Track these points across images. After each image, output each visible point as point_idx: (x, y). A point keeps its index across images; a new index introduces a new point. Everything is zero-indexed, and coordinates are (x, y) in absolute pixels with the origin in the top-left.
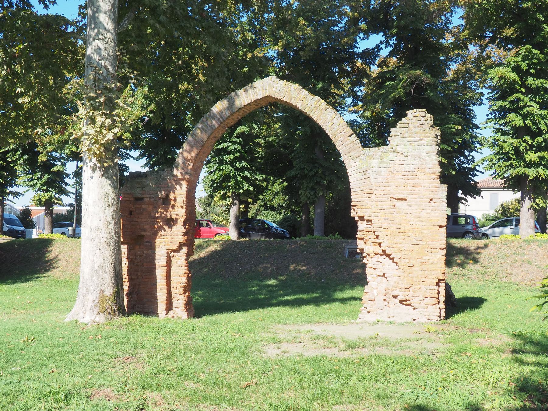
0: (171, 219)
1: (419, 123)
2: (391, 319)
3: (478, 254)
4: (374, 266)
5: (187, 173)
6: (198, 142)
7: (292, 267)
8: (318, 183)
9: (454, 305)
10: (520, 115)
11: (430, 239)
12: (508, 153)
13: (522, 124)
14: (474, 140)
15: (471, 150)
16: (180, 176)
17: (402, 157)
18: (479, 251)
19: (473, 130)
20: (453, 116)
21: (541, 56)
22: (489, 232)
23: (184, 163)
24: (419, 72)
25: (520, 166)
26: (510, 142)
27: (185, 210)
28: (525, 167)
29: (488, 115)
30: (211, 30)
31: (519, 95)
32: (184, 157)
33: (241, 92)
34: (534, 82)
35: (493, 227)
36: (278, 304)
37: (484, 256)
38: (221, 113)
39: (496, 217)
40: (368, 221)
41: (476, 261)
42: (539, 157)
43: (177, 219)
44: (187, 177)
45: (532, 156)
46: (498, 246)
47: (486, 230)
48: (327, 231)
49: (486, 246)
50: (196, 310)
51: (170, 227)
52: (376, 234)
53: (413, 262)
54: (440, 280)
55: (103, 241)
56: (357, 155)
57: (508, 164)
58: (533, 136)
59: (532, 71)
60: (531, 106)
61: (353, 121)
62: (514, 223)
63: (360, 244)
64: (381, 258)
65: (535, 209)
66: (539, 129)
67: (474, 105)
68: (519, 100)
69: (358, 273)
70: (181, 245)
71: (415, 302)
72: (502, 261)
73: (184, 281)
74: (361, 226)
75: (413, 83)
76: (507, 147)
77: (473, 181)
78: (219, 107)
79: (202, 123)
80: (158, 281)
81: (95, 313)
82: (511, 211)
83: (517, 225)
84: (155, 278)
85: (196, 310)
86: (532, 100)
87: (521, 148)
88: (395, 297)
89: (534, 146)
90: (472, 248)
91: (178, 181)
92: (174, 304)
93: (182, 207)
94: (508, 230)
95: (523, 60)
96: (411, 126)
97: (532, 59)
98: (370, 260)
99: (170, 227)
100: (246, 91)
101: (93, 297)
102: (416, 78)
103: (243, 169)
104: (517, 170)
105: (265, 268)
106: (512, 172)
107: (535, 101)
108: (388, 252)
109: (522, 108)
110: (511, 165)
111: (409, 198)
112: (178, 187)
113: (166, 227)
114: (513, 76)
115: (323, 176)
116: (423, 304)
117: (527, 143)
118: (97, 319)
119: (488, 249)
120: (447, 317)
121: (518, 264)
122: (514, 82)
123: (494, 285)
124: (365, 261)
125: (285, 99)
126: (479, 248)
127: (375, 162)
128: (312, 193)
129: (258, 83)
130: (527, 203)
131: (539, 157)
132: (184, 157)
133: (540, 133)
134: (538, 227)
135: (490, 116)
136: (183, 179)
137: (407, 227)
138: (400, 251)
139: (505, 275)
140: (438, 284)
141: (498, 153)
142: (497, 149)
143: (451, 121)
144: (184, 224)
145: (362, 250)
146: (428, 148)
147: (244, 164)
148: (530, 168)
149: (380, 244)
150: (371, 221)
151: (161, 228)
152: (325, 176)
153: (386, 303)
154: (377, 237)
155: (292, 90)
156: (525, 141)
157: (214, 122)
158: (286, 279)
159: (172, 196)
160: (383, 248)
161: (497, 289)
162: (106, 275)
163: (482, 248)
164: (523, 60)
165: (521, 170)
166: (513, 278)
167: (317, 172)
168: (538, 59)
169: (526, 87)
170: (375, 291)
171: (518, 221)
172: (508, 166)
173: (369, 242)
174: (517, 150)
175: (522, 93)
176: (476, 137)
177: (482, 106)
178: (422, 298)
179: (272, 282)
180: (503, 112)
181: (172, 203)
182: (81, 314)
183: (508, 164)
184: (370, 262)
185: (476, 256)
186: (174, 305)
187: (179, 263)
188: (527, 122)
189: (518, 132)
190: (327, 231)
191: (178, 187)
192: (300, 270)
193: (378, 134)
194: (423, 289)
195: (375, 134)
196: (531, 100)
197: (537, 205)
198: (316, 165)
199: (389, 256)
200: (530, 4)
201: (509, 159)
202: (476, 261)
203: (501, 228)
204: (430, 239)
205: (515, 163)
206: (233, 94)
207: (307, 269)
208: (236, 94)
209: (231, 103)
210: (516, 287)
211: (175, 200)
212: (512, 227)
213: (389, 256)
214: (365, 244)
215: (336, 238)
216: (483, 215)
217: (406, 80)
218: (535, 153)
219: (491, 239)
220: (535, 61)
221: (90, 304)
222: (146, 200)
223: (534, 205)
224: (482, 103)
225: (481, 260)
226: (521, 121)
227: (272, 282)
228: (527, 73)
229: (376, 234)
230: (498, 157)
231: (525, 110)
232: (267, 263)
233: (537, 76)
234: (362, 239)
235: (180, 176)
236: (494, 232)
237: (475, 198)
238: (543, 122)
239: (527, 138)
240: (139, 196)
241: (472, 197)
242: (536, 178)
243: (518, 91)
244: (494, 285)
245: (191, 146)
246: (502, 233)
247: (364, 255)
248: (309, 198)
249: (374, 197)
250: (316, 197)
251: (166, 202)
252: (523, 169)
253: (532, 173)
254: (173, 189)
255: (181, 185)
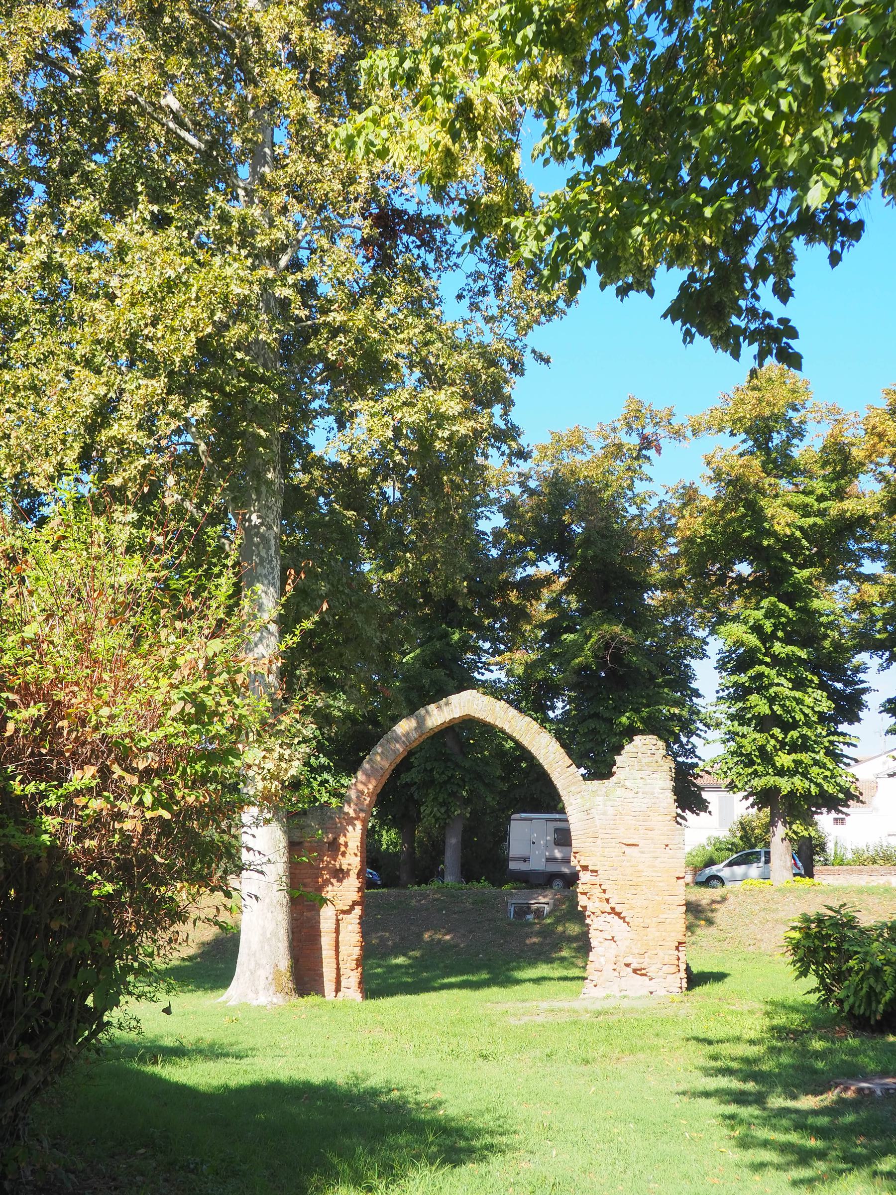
0: (341, 870)
1: (649, 752)
2: (624, 993)
3: (713, 911)
4: (599, 928)
5: (361, 810)
6: (377, 770)
7: (426, 936)
8: (453, 794)
9: (694, 980)
10: (765, 697)
11: (667, 893)
12: (750, 754)
13: (768, 712)
14: (695, 717)
15: (690, 733)
16: (352, 814)
17: (632, 794)
18: (715, 906)
19: (691, 700)
20: (666, 690)
21: (791, 614)
22: (725, 873)
23: (358, 797)
24: (617, 629)
25: (768, 774)
26: (752, 738)
27: (359, 859)
28: (775, 775)
29: (718, 692)
30: (363, 606)
31: (762, 668)
32: (358, 791)
33: (432, 707)
34: (782, 650)
35: (730, 864)
36: (435, 989)
37: (721, 916)
38: (407, 735)
39: (733, 844)
40: (592, 871)
41: (710, 922)
42: (794, 761)
43: (349, 870)
44: (362, 815)
45: (784, 760)
46: (741, 898)
47: (719, 871)
48: (468, 874)
49: (724, 899)
50: (373, 988)
51: (340, 880)
52: (603, 887)
53: (648, 921)
54: (680, 943)
55: (275, 901)
56: (578, 790)
57: (750, 770)
58: (787, 727)
59: (780, 634)
60: (778, 685)
61: (495, 682)
62: (763, 859)
63: (582, 900)
64: (610, 918)
65: (791, 840)
66: (793, 718)
67: (692, 657)
68: (760, 675)
69: (534, 943)
70: (355, 904)
71: (652, 971)
72: (747, 921)
73: (356, 952)
74: (584, 877)
75: (607, 646)
76: (748, 748)
77: (695, 785)
78: (404, 727)
79: (382, 746)
80: (324, 952)
81: (271, 993)
82: (756, 831)
83: (767, 861)
84: (320, 949)
85: (373, 988)
86: (781, 675)
87: (769, 748)
88: (628, 965)
89: (786, 744)
90: (704, 902)
91: (351, 821)
92: (344, 983)
93: (356, 855)
94: (754, 870)
95: (767, 616)
96: (640, 755)
97: (779, 616)
98: (595, 920)
99: (340, 880)
100: (439, 707)
101: (264, 973)
102: (613, 639)
103: (323, 768)
104: (764, 780)
105: (381, 938)
106: (759, 783)
107: (785, 677)
108: (617, 910)
109: (767, 688)
110: (755, 773)
111: (641, 843)
112: (350, 828)
113: (334, 881)
114: (753, 640)
115: (461, 783)
116: (660, 973)
117: (776, 739)
118: (275, 1000)
119: (726, 904)
120: (688, 989)
121: (770, 925)
122: (753, 651)
123: (739, 957)
124: (588, 921)
125: (488, 720)
126: (714, 902)
127: (599, 800)
128: (443, 810)
129: (454, 698)
130: (780, 830)
131: (794, 761)
132: (358, 791)
133: (795, 725)
134: (800, 864)
135: (721, 694)
136: (357, 818)
137: (640, 879)
138: (632, 908)
139: (752, 942)
140: (677, 948)
141: (733, 753)
142: (732, 745)
143: (663, 698)
144: (358, 876)
145: (585, 908)
146: (661, 784)
147: (323, 760)
148: (782, 776)
149: (607, 901)
150: (596, 871)
151: (327, 882)
152: (464, 781)
153: (616, 974)
154: (604, 891)
155: (498, 709)
156: (773, 736)
157: (398, 746)
158: (422, 956)
159: (342, 840)
160: (612, 905)
161: (742, 962)
162: (280, 945)
163: (719, 902)
164: (767, 616)
165: (771, 780)
166: (764, 946)
167: (453, 776)
168: (787, 617)
169: (774, 657)
170: (602, 959)
171: (768, 854)
172: (750, 774)
173: (594, 898)
174: (762, 749)
175: (767, 665)
176: (698, 713)
177: (705, 659)
178: (660, 966)
179: (400, 960)
180: (741, 693)
181: (342, 849)
182: (251, 995)
183: (750, 770)
184: (594, 923)
185: (710, 915)
186: (343, 984)
187: (350, 927)
188: (775, 708)
189: (763, 724)
190: (468, 874)
191: (350, 828)
192: (439, 940)
193: (533, 701)
194: (661, 954)
195: (598, 764)
196: (779, 674)
197: (795, 832)
198: (449, 764)
199: (618, 914)
200: (772, 541)
201: (751, 763)
202: (710, 922)
203: (743, 867)
204: (667, 893)
205: (760, 769)
206: (422, 711)
207: (452, 939)
208: (427, 712)
209: (421, 722)
210: (768, 958)
211: (346, 845)
212: (761, 864)
213: (618, 914)
214: (588, 900)
215: (483, 887)
216: (709, 838)
217: (598, 640)
218: (789, 754)
219: (729, 886)
220: (783, 620)
221: (262, 983)
222: (306, 844)
223: (790, 833)
224: (705, 655)
225: (717, 920)
226: (767, 707)
227: (400, 960)
228: (773, 636)
229: (603, 887)
230: (736, 759)
231: (772, 691)
232: (384, 930)
233: (787, 641)
234: (585, 894)
235: (352, 814)
236: (733, 874)
237: (698, 814)
238: (797, 709)
239: (776, 731)
240: (298, 840)
241: (693, 812)
242: (792, 793)
243: (761, 663)
244: (739, 957)
245: (368, 776)
246: (745, 877)
247: (587, 913)
248: (437, 820)
249: (599, 842)
250: (449, 817)
251: (334, 847)
252: (773, 778)
253: (785, 785)
254: (344, 831)
255: (354, 825)
